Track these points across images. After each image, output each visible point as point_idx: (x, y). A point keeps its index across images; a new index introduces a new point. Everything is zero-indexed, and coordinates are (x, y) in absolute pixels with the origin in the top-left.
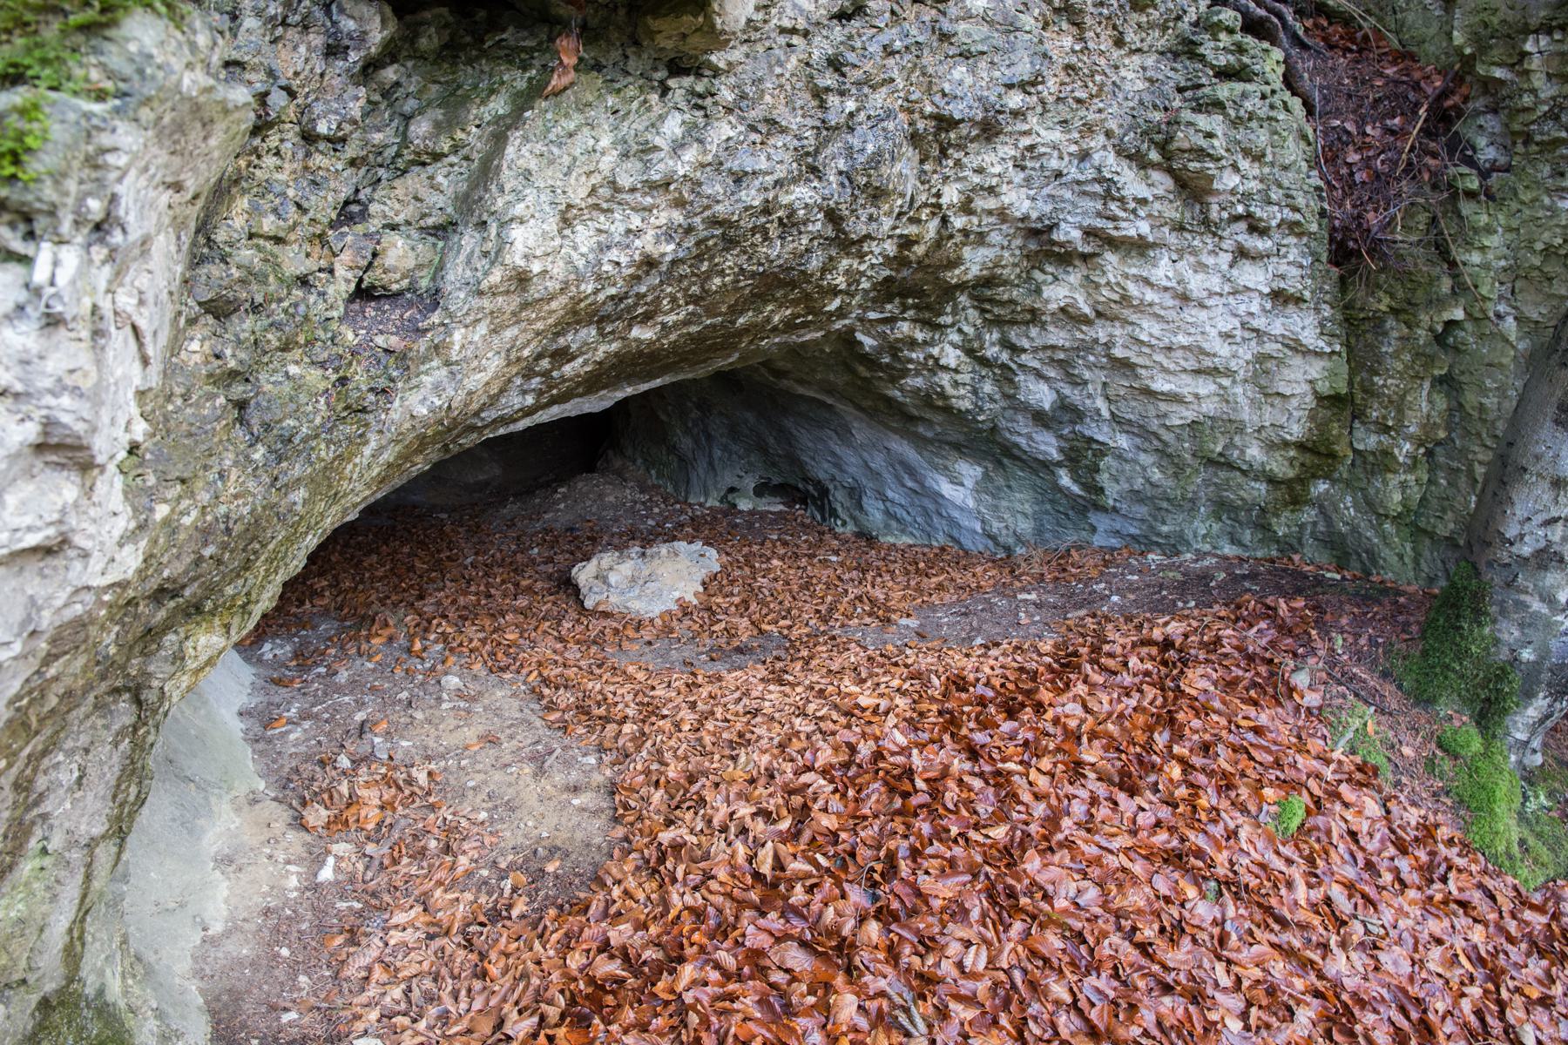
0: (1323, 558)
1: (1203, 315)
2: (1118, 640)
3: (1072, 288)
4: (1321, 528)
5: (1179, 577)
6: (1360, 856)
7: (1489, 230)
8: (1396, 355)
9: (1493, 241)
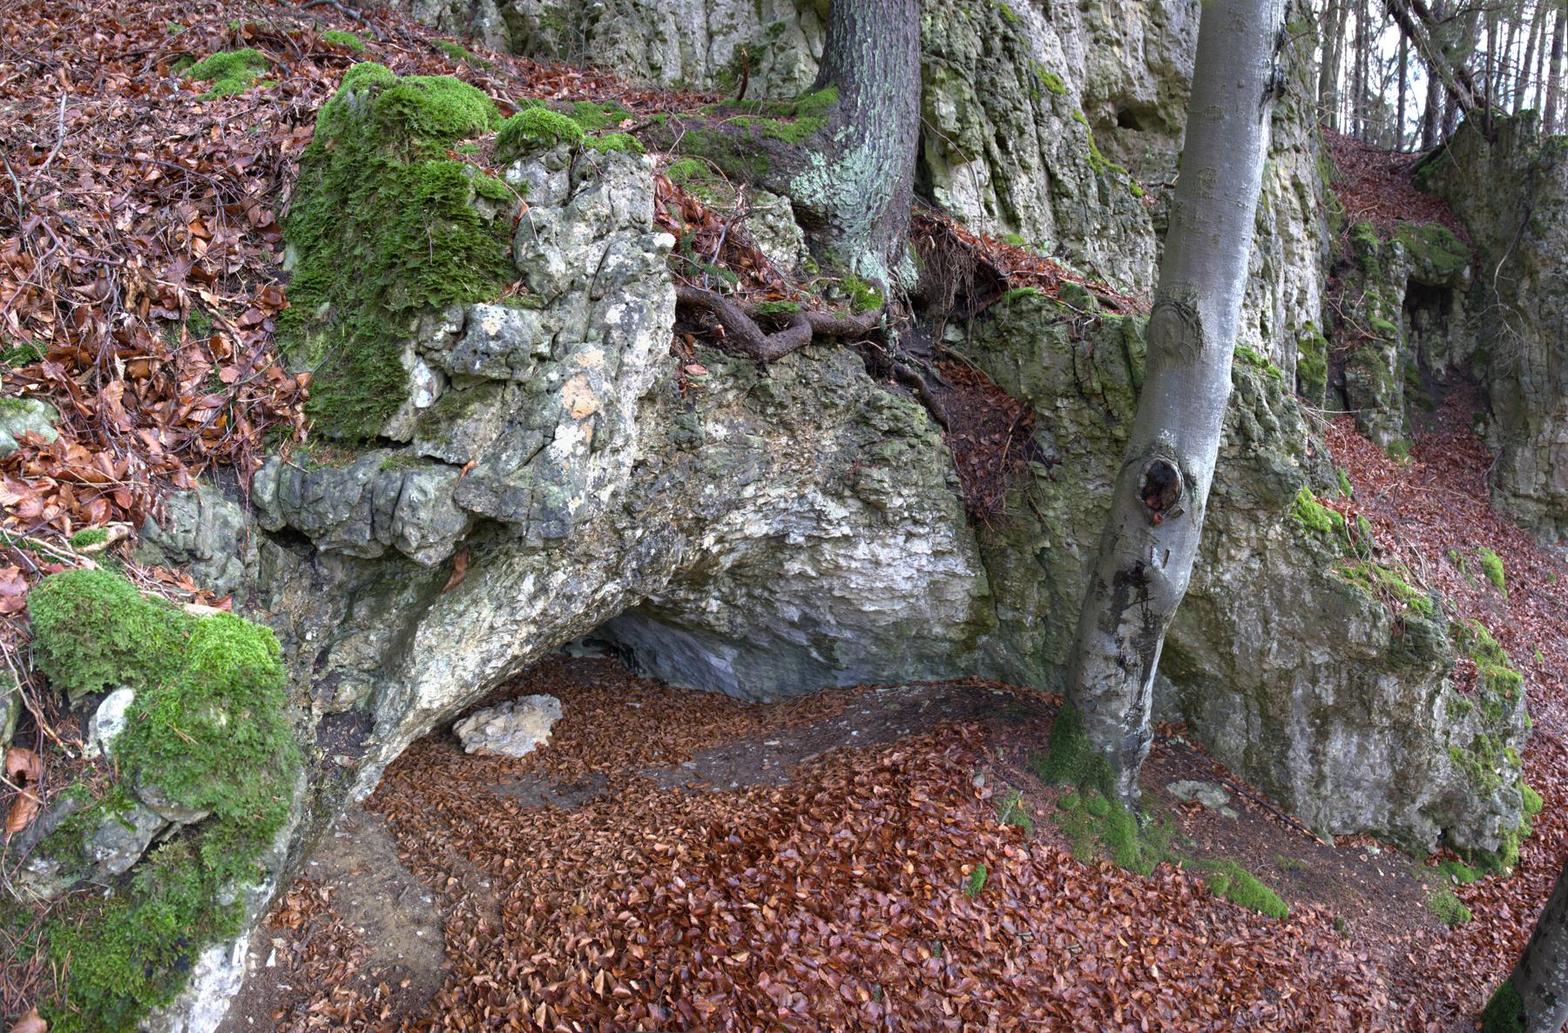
0: (992, 677)
1: (891, 570)
2: (863, 770)
3: (803, 563)
4: (987, 660)
5: (898, 707)
6: (1018, 891)
7: (1056, 499)
8: (1016, 569)
9: (1059, 504)
